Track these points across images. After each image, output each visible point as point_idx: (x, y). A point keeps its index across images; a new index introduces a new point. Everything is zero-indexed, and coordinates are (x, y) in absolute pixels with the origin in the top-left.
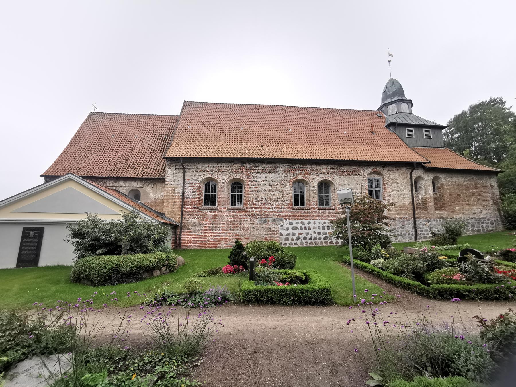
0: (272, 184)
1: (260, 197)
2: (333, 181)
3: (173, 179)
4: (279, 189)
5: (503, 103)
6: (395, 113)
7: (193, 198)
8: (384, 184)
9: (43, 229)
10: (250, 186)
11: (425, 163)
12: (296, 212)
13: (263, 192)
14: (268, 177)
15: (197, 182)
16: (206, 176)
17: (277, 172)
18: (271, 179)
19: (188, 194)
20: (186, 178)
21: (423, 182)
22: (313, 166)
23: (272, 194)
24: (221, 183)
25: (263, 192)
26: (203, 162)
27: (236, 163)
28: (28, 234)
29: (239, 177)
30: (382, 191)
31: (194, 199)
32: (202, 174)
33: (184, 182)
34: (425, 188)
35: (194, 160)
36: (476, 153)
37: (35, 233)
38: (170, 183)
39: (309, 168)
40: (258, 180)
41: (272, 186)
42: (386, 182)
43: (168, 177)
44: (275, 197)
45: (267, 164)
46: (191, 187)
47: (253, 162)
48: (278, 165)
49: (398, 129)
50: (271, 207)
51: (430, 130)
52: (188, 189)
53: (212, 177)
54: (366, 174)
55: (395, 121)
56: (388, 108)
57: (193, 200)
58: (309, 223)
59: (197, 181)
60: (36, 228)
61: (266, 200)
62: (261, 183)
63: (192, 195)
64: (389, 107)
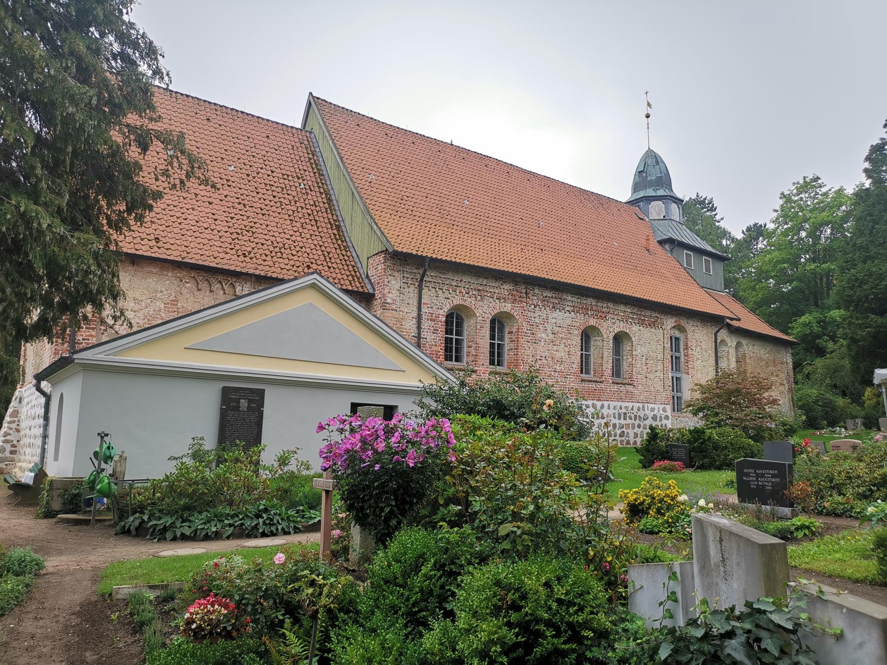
0: (556, 329)
1: (538, 353)
2: (631, 335)
3: (398, 300)
4: (564, 341)
5: (713, 209)
6: (662, 217)
7: (434, 343)
8: (687, 348)
9: (261, 393)
10: (525, 330)
11: (732, 319)
12: (586, 385)
13: (542, 344)
14: (550, 317)
15: (441, 312)
16: (457, 301)
17: (564, 309)
18: (554, 321)
19: (426, 334)
20: (423, 301)
21: (726, 349)
22: (609, 304)
23: (555, 348)
24: (481, 318)
25: (542, 344)
26: (479, 277)
27: (505, 282)
28: (235, 404)
29: (509, 311)
30: (682, 360)
31: (436, 346)
32: (449, 296)
33: (419, 309)
34: (728, 359)
35: (437, 264)
36: (771, 314)
37: (250, 401)
38: (394, 307)
39: (604, 306)
40: (537, 320)
41: (554, 334)
42: (690, 344)
43: (389, 292)
44: (558, 355)
45: (551, 291)
46: (431, 320)
47: (530, 284)
48: (565, 296)
49: (677, 251)
50: (553, 373)
51: (692, 254)
52: (425, 324)
53: (466, 304)
54: (669, 328)
55: (675, 237)
56: (650, 206)
57: (434, 348)
58: (602, 407)
59: (441, 309)
60: (252, 391)
61: (547, 360)
62: (540, 327)
63: (433, 337)
64: (653, 203)
